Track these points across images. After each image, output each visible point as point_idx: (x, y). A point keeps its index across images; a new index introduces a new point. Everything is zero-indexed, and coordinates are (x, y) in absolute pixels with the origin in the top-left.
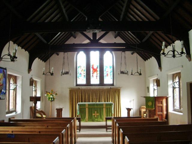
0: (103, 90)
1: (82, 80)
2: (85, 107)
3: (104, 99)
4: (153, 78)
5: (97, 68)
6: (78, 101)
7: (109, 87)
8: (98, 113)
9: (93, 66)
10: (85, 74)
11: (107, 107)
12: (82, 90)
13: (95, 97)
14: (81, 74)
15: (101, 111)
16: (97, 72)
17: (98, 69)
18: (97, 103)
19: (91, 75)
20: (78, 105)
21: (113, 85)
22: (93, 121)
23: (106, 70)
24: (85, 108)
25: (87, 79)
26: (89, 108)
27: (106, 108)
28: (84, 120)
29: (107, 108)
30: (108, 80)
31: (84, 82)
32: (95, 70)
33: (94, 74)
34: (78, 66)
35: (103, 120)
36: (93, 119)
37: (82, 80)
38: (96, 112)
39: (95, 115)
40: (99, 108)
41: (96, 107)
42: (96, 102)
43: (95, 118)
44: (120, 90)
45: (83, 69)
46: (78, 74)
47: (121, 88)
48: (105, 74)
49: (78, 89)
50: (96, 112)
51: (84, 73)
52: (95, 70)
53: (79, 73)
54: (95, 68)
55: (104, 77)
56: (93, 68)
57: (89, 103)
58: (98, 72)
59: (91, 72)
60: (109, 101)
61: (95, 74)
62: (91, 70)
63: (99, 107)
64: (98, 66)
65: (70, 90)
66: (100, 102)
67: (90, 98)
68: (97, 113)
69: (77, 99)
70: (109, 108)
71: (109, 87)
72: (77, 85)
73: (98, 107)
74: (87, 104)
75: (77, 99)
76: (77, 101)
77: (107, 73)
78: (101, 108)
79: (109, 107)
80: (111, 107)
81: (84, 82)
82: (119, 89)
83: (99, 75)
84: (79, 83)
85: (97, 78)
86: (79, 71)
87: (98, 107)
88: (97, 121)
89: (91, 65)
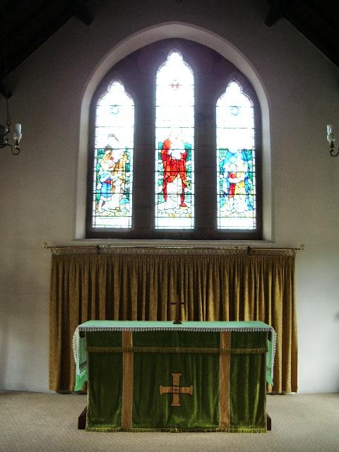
0: (218, 261)
1: (114, 213)
2: (115, 349)
3: (214, 301)
4: (75, 368)
5: (185, 157)
6: (84, 315)
7: (243, 245)
8: (188, 384)
9: (165, 147)
10: (130, 186)
11: (238, 351)
12: (110, 256)
13: (173, 291)
14: (108, 182)
15: (205, 376)
16: (183, 178)
17: (190, 164)
18: (186, 325)
19: (158, 189)
20: (82, 334)
21: (257, 234)
22: (161, 426)
23: (228, 168)
24: (120, 355)
25: (136, 207)
26: (139, 357)
27: (233, 355)
28: (109, 422)
29: (242, 356)
30: (235, 214)
31: (124, 221)
32: (174, 168)
33: (169, 185)
34: (100, 143)
35: (216, 422)
36: (162, 416)
37: (114, 213)
38: (176, 377)
39: (171, 395)
40: (193, 354)
41: (178, 349)
42: (178, 321)
43: (171, 408)
44: (293, 258)
45: (122, 163)
46: (100, 185)
47: (298, 254)
48: (222, 185)
49: (95, 251)
50: (176, 377)
51: (124, 180)
52: (174, 168)
53: (103, 180)
54: (176, 155)
55: (218, 198)
56: (165, 156)
57: (236, 325)
58: (191, 177)
59: (158, 177)
60: (242, 319)
61: (175, 186)
62: (159, 165)
63: (197, 350)
64: (187, 150)
65: (54, 257)
66: (197, 319)
67: (152, 297)
68: (186, 381)
69: (85, 302)
70: (252, 356)
71: (243, 245)
72: (91, 233)
73: (190, 350)
74: (127, 332)
75: (85, 302)
76: (84, 310)
77: (231, 180)
78: (205, 356)
79: (249, 350)
80: (260, 350)
81: (124, 221)
82: (291, 253)
83: (191, 189)
84: (99, 223)
85: (182, 205)
86: (103, 167)
87: (190, 350)
88: (184, 429)
89: (160, 138)
